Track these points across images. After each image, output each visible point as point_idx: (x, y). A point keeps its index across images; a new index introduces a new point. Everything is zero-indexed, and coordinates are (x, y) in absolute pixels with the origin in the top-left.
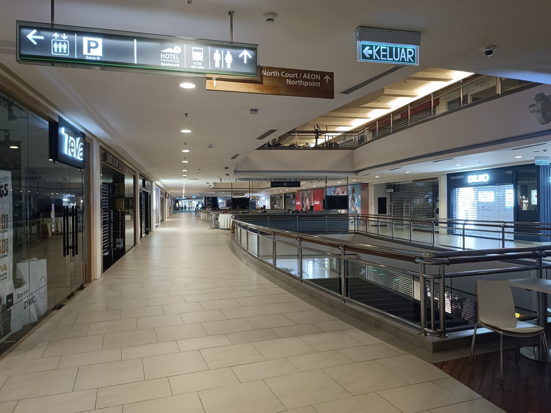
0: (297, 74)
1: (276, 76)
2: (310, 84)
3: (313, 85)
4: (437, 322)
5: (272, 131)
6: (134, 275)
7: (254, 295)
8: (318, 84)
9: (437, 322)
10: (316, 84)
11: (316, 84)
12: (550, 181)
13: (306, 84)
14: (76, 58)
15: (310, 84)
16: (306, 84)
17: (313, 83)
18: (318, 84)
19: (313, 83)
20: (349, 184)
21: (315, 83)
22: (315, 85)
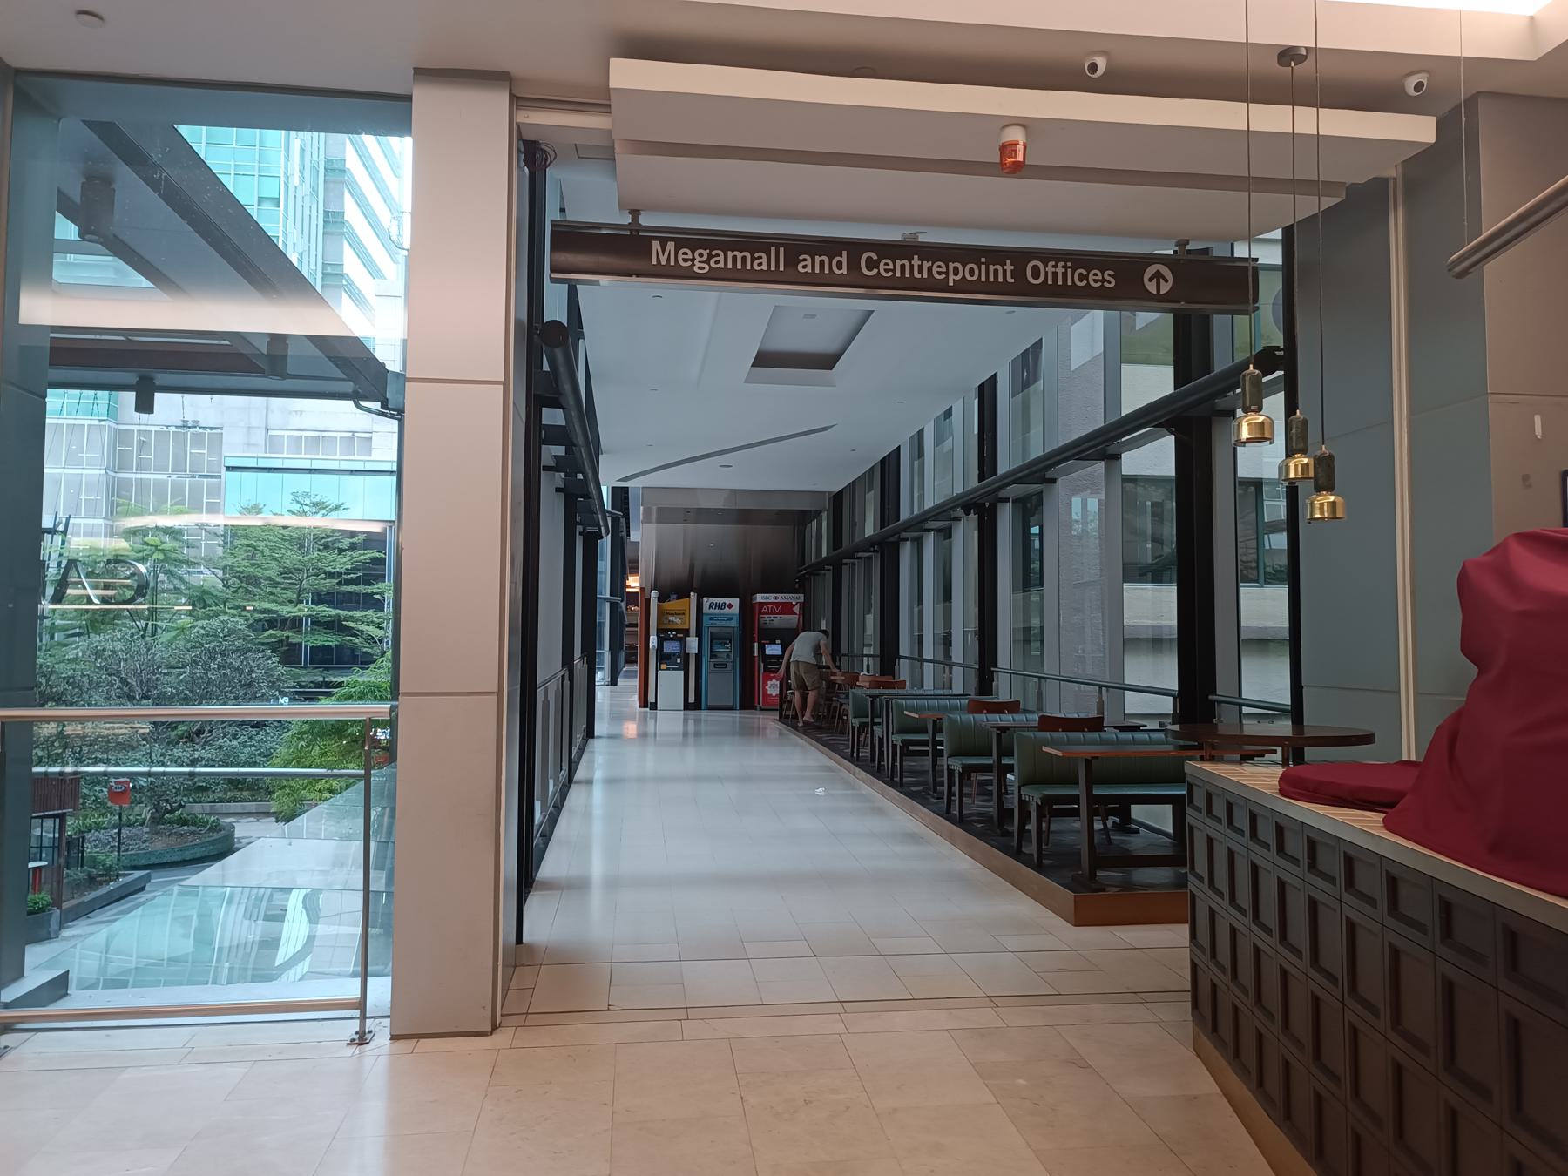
0: (1009, 267)
1: (925, 276)
2: (972, 272)
3: (983, 279)
4: (305, 656)
5: (1367, 739)
6: (1329, 1091)
7: (1057, 991)
8: (1005, 272)
9: (305, 656)
10: (996, 271)
11: (996, 271)
12: (366, 134)
13: (956, 271)
14: (1465, 699)
15: (972, 272)
16: (956, 271)
17: (983, 267)
18: (1005, 272)
19: (983, 267)
20: (941, 658)
21: (992, 268)
22: (991, 279)
